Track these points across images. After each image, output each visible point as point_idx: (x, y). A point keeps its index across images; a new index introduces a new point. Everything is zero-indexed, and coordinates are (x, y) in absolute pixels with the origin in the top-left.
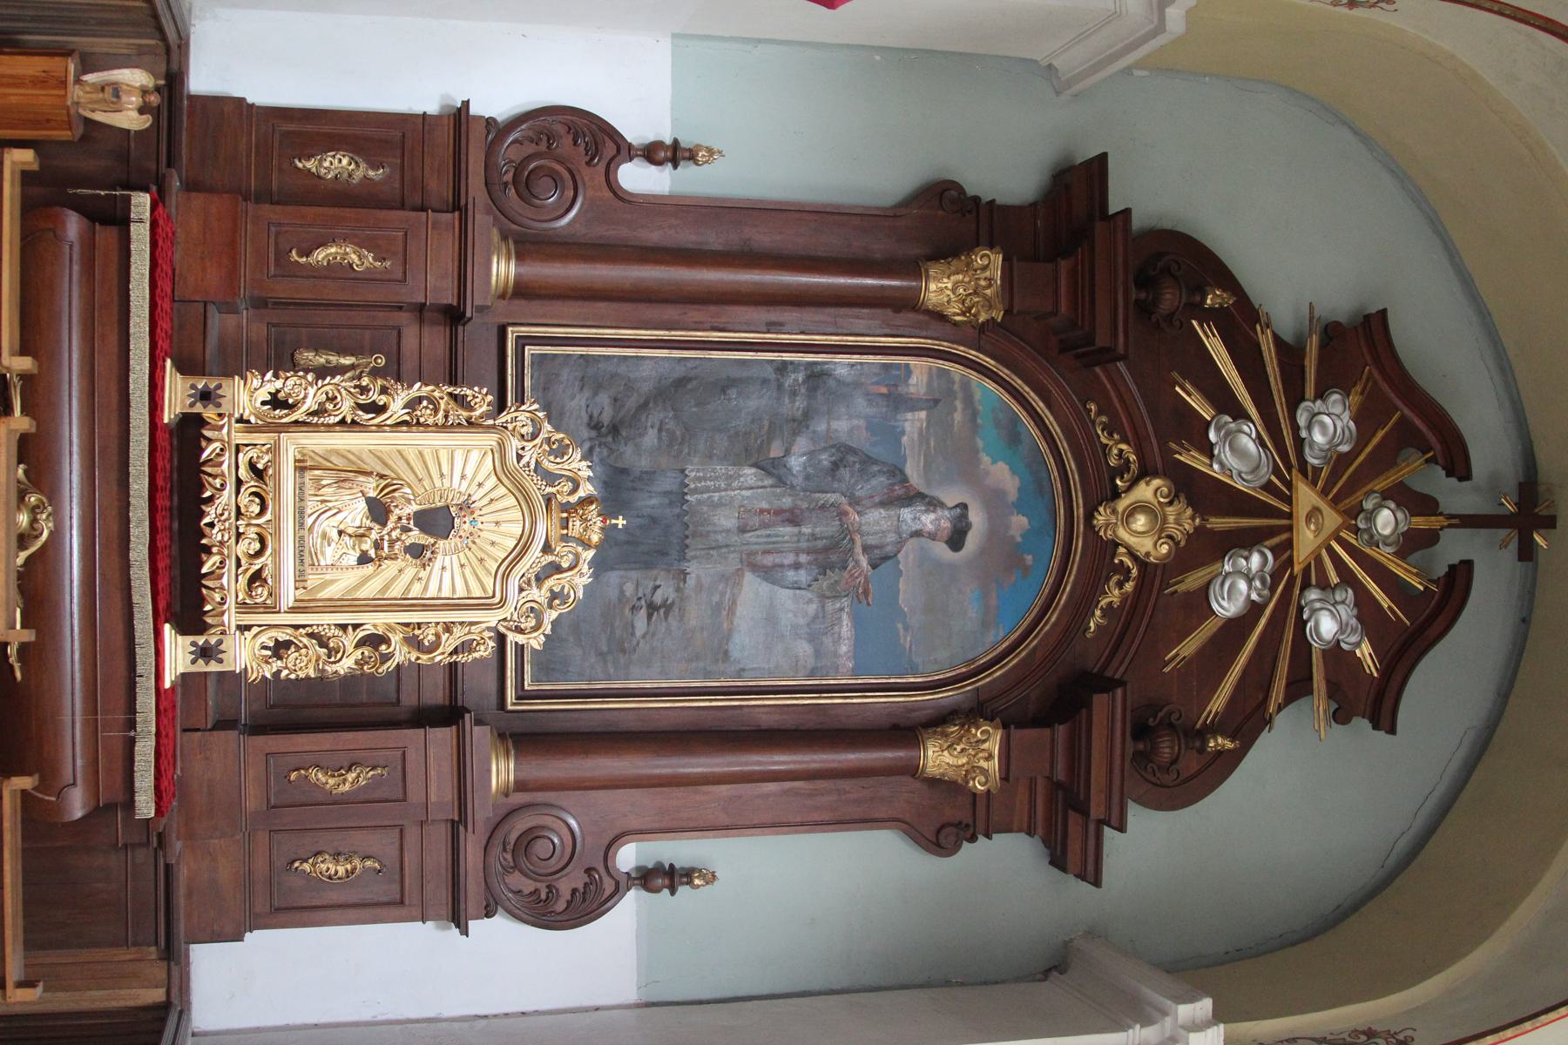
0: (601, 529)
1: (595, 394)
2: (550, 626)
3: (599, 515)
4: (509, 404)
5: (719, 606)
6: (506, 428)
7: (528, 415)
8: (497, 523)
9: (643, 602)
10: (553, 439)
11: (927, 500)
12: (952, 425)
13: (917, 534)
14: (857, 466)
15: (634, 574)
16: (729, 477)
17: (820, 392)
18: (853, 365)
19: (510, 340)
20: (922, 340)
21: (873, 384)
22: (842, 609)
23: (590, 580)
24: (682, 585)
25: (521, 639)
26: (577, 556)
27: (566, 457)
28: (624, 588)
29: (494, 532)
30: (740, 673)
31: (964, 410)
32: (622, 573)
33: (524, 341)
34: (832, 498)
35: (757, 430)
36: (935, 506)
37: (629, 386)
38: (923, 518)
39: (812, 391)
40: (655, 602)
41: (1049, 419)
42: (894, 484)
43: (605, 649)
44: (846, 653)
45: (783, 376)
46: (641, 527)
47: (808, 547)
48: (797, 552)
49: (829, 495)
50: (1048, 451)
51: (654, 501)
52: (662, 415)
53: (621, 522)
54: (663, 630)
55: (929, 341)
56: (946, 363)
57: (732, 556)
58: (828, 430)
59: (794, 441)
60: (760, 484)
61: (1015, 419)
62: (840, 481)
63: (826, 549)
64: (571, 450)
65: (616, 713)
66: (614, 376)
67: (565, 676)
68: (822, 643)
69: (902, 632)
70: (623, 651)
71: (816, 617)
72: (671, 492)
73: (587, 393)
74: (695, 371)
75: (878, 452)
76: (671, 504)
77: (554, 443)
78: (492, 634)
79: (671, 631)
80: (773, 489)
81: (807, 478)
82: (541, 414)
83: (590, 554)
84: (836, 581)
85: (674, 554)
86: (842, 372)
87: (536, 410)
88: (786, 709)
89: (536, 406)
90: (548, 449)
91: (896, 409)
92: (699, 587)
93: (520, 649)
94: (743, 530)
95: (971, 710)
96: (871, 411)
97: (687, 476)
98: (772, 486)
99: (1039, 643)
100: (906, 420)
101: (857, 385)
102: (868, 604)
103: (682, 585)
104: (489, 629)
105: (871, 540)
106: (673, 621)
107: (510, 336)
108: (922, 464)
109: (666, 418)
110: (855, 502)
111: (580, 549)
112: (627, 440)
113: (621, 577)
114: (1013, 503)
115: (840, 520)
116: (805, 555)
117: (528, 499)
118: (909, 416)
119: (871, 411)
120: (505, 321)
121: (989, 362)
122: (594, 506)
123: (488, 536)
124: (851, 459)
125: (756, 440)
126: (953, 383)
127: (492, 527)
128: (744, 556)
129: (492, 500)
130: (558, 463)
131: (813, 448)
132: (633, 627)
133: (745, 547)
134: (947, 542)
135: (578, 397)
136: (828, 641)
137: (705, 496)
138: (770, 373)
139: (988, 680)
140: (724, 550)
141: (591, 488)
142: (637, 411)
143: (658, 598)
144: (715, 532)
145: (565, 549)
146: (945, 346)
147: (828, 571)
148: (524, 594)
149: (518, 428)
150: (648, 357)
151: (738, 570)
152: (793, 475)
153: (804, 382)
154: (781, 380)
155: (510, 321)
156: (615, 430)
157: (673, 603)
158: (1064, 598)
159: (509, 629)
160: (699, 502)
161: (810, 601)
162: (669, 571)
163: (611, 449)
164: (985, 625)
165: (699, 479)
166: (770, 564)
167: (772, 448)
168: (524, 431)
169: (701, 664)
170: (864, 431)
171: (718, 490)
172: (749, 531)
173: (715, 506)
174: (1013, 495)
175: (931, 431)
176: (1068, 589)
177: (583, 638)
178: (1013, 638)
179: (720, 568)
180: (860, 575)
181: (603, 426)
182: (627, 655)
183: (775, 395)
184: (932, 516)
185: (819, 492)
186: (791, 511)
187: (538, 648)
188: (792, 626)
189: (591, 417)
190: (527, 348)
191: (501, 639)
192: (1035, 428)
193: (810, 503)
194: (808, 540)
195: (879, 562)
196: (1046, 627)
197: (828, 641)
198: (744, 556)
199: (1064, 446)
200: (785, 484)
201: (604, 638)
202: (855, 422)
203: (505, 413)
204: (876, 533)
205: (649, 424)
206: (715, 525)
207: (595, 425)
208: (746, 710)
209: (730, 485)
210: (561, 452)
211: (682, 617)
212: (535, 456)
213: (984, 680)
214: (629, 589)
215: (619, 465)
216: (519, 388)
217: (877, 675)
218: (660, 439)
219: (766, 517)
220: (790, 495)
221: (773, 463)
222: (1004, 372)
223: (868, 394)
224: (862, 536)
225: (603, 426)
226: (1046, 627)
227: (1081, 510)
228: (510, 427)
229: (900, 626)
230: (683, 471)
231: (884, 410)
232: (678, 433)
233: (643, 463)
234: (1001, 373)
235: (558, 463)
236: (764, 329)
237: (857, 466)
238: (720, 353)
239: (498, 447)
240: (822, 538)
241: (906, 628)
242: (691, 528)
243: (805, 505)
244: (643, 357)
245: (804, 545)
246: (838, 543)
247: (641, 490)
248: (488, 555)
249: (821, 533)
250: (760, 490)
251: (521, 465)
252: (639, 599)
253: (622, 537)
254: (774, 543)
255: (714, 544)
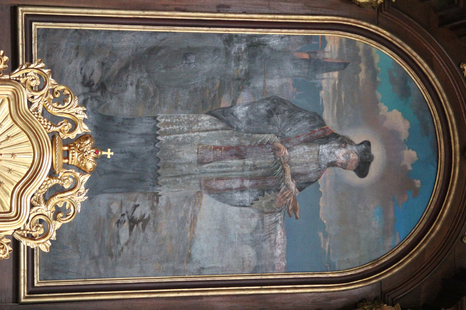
0: (95, 158)
1: (87, 60)
2: (55, 234)
3: (93, 148)
4: (21, 63)
5: (183, 222)
6: (19, 81)
7: (36, 71)
8: (13, 155)
9: (126, 217)
10: (56, 90)
11: (340, 138)
12: (358, 82)
13: (333, 164)
14: (287, 113)
15: (119, 197)
16: (190, 123)
17: (258, 58)
18: (282, 37)
19: (20, 17)
20: (335, 18)
21: (298, 51)
22: (276, 222)
23: (86, 198)
24: (155, 204)
25: (32, 244)
26: (76, 180)
27: (66, 104)
28: (112, 207)
29: (10, 161)
30: (200, 271)
31: (366, 71)
32: (110, 195)
33: (31, 19)
34: (268, 137)
35: (210, 87)
36: (346, 144)
37: (113, 54)
38: (337, 152)
39: (252, 57)
40: (135, 218)
41: (432, 76)
42: (314, 127)
43: (96, 253)
44: (280, 255)
45: (230, 46)
46: (124, 160)
47: (251, 175)
48: (242, 179)
49: (266, 135)
50: (431, 101)
51: (133, 141)
52: (138, 76)
53: (109, 153)
54: (142, 239)
55: (340, 18)
56: (353, 35)
57: (193, 182)
58: (264, 87)
59: (239, 94)
60: (214, 127)
61: (405, 77)
62: (274, 125)
63: (264, 177)
64: (70, 99)
65: (106, 303)
66: (101, 46)
67: (66, 275)
68: (262, 248)
69: (322, 238)
70: (111, 255)
71: (257, 228)
72: (146, 134)
73: (81, 59)
74: (164, 42)
75: (302, 102)
76: (147, 143)
77: (57, 93)
78: (9, 241)
79: (147, 239)
80: (223, 131)
81: (249, 122)
82: (46, 71)
83: (86, 178)
84: (272, 200)
85: (149, 181)
86: (274, 43)
87: (42, 68)
88: (235, 298)
89: (42, 65)
90: (52, 98)
91: (316, 70)
92: (169, 206)
93: (31, 252)
94: (201, 162)
95: (376, 299)
96: (296, 72)
97: (158, 122)
98: (222, 129)
99: (427, 246)
100: (323, 79)
101: (285, 52)
102: (297, 218)
103: (155, 204)
104: (7, 237)
105: (298, 169)
106: (149, 232)
107: (20, 14)
108: (335, 111)
109: (142, 77)
110: (285, 140)
111: (78, 174)
112: (112, 94)
113: (109, 199)
114: (405, 140)
115: (274, 154)
116: (248, 181)
117: (37, 136)
118: (325, 75)
119: (296, 72)
120: (16, 3)
121: (386, 34)
122: (88, 141)
123: (5, 165)
124: (282, 108)
125: (210, 93)
126: (358, 50)
127: (9, 158)
128: (202, 182)
129: (8, 137)
130: (60, 109)
131: (253, 100)
132: (118, 237)
133: (203, 176)
134: (355, 171)
135: (74, 62)
136: (266, 245)
137: (172, 137)
138: (220, 43)
139: (389, 275)
140: (186, 178)
141: (86, 127)
142: (119, 72)
143: (137, 214)
144: (180, 164)
145: (67, 174)
146: (352, 22)
147: (266, 193)
148: (34, 209)
149: (28, 81)
150: (127, 32)
151: (198, 192)
152: (239, 121)
153: (245, 50)
154: (229, 49)
155: (20, 3)
156: (103, 87)
157: (149, 217)
158: (446, 212)
159: (23, 237)
160: (168, 142)
161: (253, 215)
162: (145, 194)
163: (99, 101)
164: (385, 232)
165: (167, 124)
166: (222, 188)
167: (223, 100)
168: (33, 84)
169: (171, 265)
170: (292, 87)
171: (182, 132)
172: (206, 163)
173: (184, 143)
174: (404, 135)
175: (342, 86)
176: (449, 205)
177: (80, 246)
178: (407, 243)
179: (184, 191)
180: (290, 196)
181: (93, 84)
182: (114, 259)
183: (224, 60)
184: (344, 151)
185: (258, 133)
186: (238, 147)
187: (46, 251)
188: (239, 235)
189: (84, 77)
190: (34, 24)
191: (16, 244)
192: (421, 83)
193: (251, 142)
194: (250, 170)
195: (304, 186)
196: (432, 234)
197: (266, 245)
198: (202, 182)
199: (443, 97)
200: (232, 127)
201: (96, 246)
202: (285, 80)
203: (18, 70)
204: (301, 164)
205: (129, 83)
206: (179, 158)
207: (87, 83)
208: (205, 299)
209: (191, 128)
210: (62, 100)
211: (155, 230)
212: (42, 103)
213: (386, 275)
214: (115, 207)
215: (106, 113)
216: (28, 55)
217: (303, 272)
218: (137, 93)
219: (219, 152)
220: (236, 136)
221: (223, 111)
222: (397, 42)
223: (294, 60)
224: (291, 166)
225: (93, 84)
226: (432, 234)
227: (458, 145)
228: (22, 80)
229: (321, 234)
230: (155, 118)
231: (307, 70)
232: (151, 89)
233: (125, 111)
234: (394, 42)
235: (60, 109)
236: (216, 10)
237: (287, 113)
238: (182, 28)
239: (13, 96)
240: (261, 168)
241: (326, 236)
242: (162, 161)
243: (248, 143)
244: (124, 31)
245: (247, 173)
246: (273, 172)
247: (124, 132)
248: (7, 180)
249: (261, 163)
250: (213, 132)
251: (31, 110)
252: (123, 215)
253: (109, 168)
254: (224, 172)
255: (179, 173)
